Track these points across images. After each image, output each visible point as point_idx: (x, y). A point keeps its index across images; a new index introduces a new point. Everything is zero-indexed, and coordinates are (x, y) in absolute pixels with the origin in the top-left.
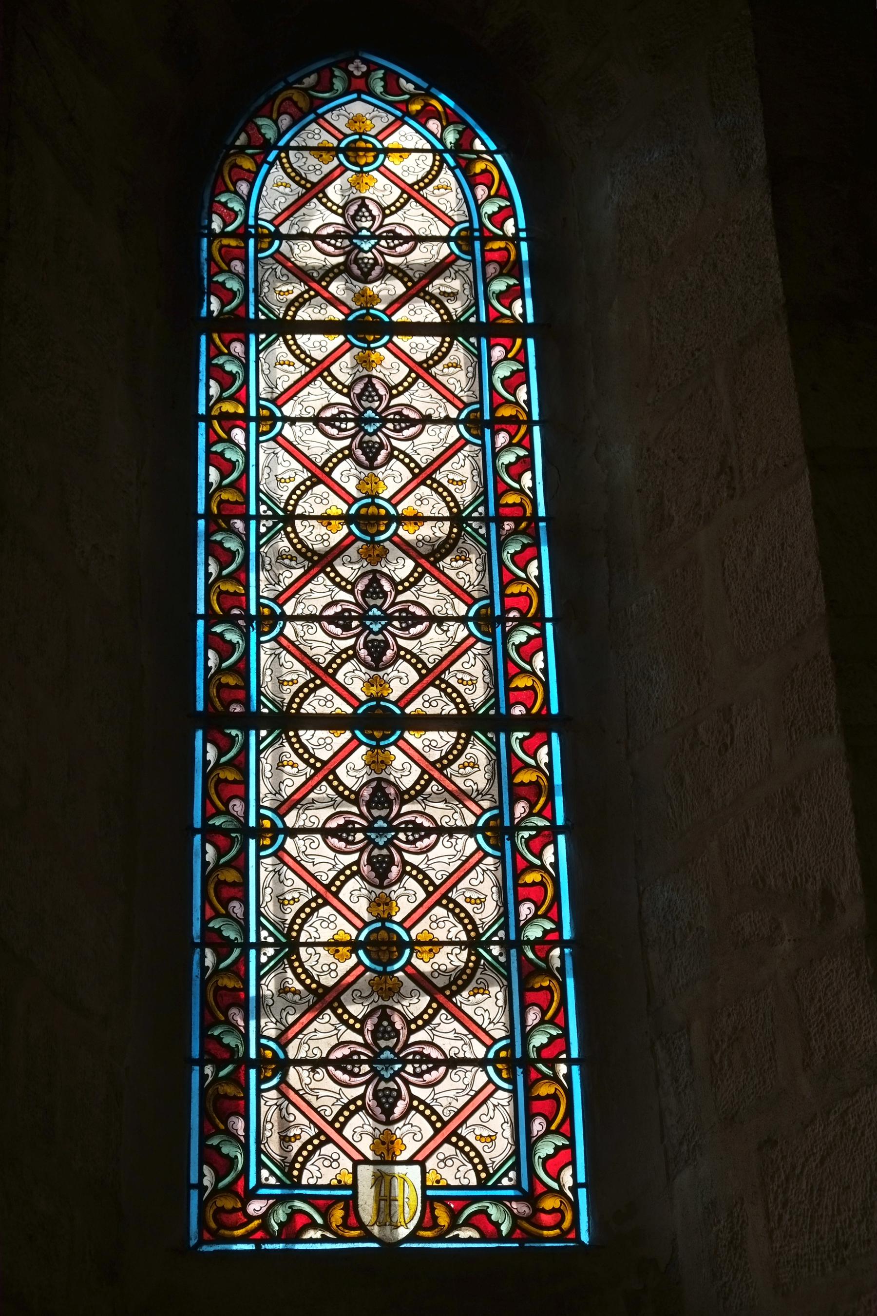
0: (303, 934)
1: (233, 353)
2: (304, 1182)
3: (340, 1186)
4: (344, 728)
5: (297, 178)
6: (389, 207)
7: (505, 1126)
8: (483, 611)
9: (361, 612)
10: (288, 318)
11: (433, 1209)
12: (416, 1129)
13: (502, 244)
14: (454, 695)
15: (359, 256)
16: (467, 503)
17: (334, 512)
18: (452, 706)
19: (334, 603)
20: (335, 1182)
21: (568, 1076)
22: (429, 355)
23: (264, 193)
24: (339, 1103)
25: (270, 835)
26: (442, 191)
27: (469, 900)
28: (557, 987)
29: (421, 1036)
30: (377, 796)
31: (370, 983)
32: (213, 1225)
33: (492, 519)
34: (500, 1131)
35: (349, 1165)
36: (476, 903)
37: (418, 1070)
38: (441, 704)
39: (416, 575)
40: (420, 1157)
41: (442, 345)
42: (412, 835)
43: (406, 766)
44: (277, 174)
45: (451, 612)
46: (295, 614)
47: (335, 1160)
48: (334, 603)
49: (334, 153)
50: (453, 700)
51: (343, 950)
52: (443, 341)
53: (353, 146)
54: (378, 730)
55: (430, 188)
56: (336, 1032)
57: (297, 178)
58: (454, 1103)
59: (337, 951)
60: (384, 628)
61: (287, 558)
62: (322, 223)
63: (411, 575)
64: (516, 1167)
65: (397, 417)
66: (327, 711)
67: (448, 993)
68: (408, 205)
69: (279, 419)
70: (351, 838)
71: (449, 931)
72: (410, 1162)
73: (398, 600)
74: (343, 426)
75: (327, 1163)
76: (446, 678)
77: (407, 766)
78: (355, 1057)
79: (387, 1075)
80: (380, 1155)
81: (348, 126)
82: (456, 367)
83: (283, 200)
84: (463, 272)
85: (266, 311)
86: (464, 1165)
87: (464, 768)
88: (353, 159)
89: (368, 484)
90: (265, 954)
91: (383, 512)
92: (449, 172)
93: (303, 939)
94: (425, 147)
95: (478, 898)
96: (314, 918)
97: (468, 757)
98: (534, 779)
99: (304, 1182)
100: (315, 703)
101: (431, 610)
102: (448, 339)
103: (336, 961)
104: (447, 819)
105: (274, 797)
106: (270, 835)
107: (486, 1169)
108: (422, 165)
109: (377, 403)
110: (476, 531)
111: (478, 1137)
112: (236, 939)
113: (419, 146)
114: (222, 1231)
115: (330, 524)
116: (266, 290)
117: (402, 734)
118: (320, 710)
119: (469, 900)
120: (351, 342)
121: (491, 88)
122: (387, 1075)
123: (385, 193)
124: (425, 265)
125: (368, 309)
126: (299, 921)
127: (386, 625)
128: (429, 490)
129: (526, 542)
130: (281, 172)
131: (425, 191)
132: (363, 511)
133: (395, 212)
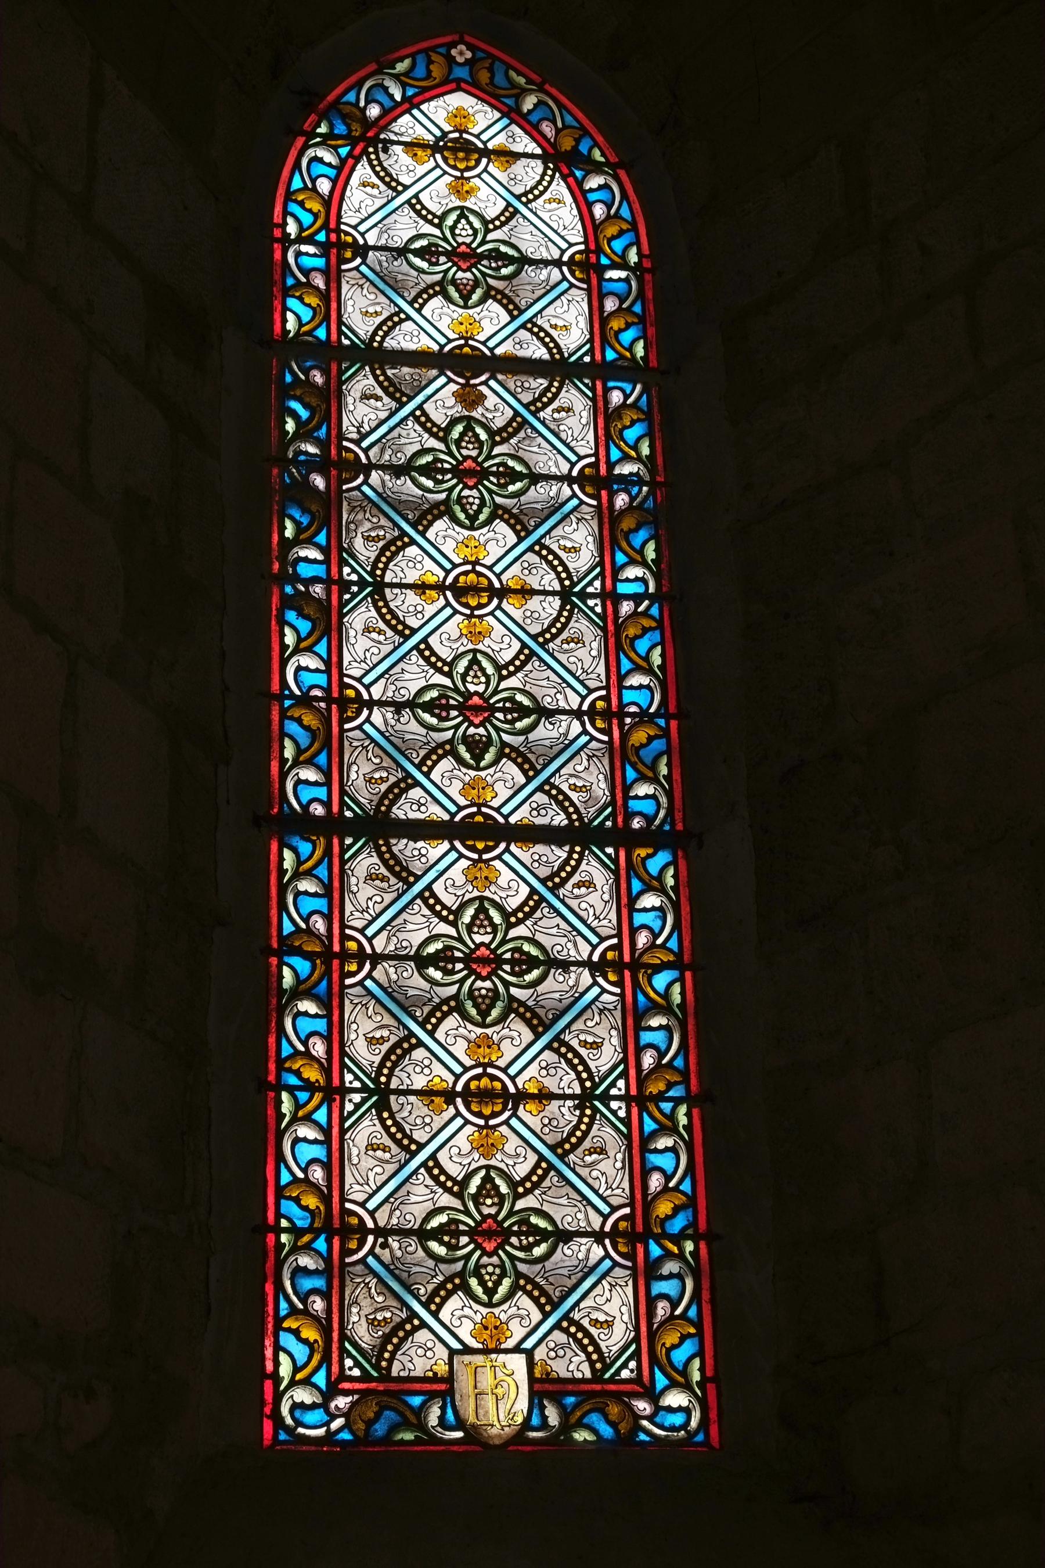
0: (396, 1364)
1: (311, 1179)
2: (394, 1373)
3: (435, 1379)
4: (442, 837)
5: (387, 179)
6: (492, 221)
7: (580, 318)
8: (587, 471)
9: (454, 463)
10: (375, 344)
11: (542, 1408)
12: (523, 1312)
13: (623, 274)
14: (556, 563)
15: (457, 276)
16: (581, 574)
17: (431, 580)
18: (563, 816)
19: (419, 236)
20: (430, 1374)
21: (695, 1254)
22: (528, 188)
23: (348, 193)
24: (435, 1280)
25: (358, 1236)
26: (554, 205)
27: (584, 1044)
28: (669, 906)
29: (529, 1202)
30: (485, 1189)
31: (465, 872)
32: (289, 1421)
33: (627, 966)
34: (618, 1315)
35: (442, 1353)
36: (591, 1048)
37: (525, 1242)
38: (551, 813)
39: (522, 657)
40: (528, 1344)
41: (570, 857)
42: (527, 1239)
43: (512, 884)
44: (364, 171)
45: (562, 704)
46: (384, 699)
47: (430, 1349)
48: (419, 236)
49: (429, 152)
50: (546, 345)
51: (438, 1100)
52: (571, 852)
53: (458, 351)
54: (481, 839)
55: (540, 201)
56: (431, 1196)
57: (387, 179)
58: (529, 295)
59: (432, 1101)
60: (487, 720)
61: (374, 631)
62: (415, 233)
63: (516, 657)
64: (636, 1355)
65: (508, 705)
66: (422, 816)
67: (560, 1151)
68: (514, 220)
69: (370, 1231)
70: (434, 260)
71: (561, 1080)
72: (517, 1349)
73: (517, 1207)
74: (440, 477)
75: (411, 564)
76: (557, 783)
77: (513, 884)
78: (444, 701)
79: (477, 721)
80: (483, 1343)
81: (463, 792)
82: (599, 1154)
83: (376, 651)
84: (609, 1010)
85: (354, 1353)
86: (577, 1355)
87: (568, 643)
88: (452, 163)
89: (474, 789)
90: (350, 1101)
91: (498, 1085)
92: (562, 183)
93: (387, 579)
94: (535, 152)
95: (594, 1042)
96: (408, 1344)
97: (554, 193)
98: (635, 470)
99: (394, 1373)
100: (400, 338)
101: (540, 700)
102: (578, 849)
103: (431, 1113)
104: (549, 700)
105: (361, 916)
106: (358, 1236)
107: (591, 1077)
108: (531, 173)
109: (471, 238)
110: (592, 609)
111: (583, 1044)
112: (317, 1081)
113: (529, 150)
114: (301, 1430)
115: (424, 593)
116: (355, 1318)
117: (508, 846)
118: (412, 815)
119: (584, 1044)
120: (457, 851)
121: (609, 104)
122: (477, 721)
123: (510, 893)
124: (560, 1001)
125: (467, 384)
126: (381, 333)
127: (489, 716)
128: (529, 334)
129: (652, 733)
130: (369, 170)
131: (533, 204)
132: (473, 1085)
133: (499, 227)
